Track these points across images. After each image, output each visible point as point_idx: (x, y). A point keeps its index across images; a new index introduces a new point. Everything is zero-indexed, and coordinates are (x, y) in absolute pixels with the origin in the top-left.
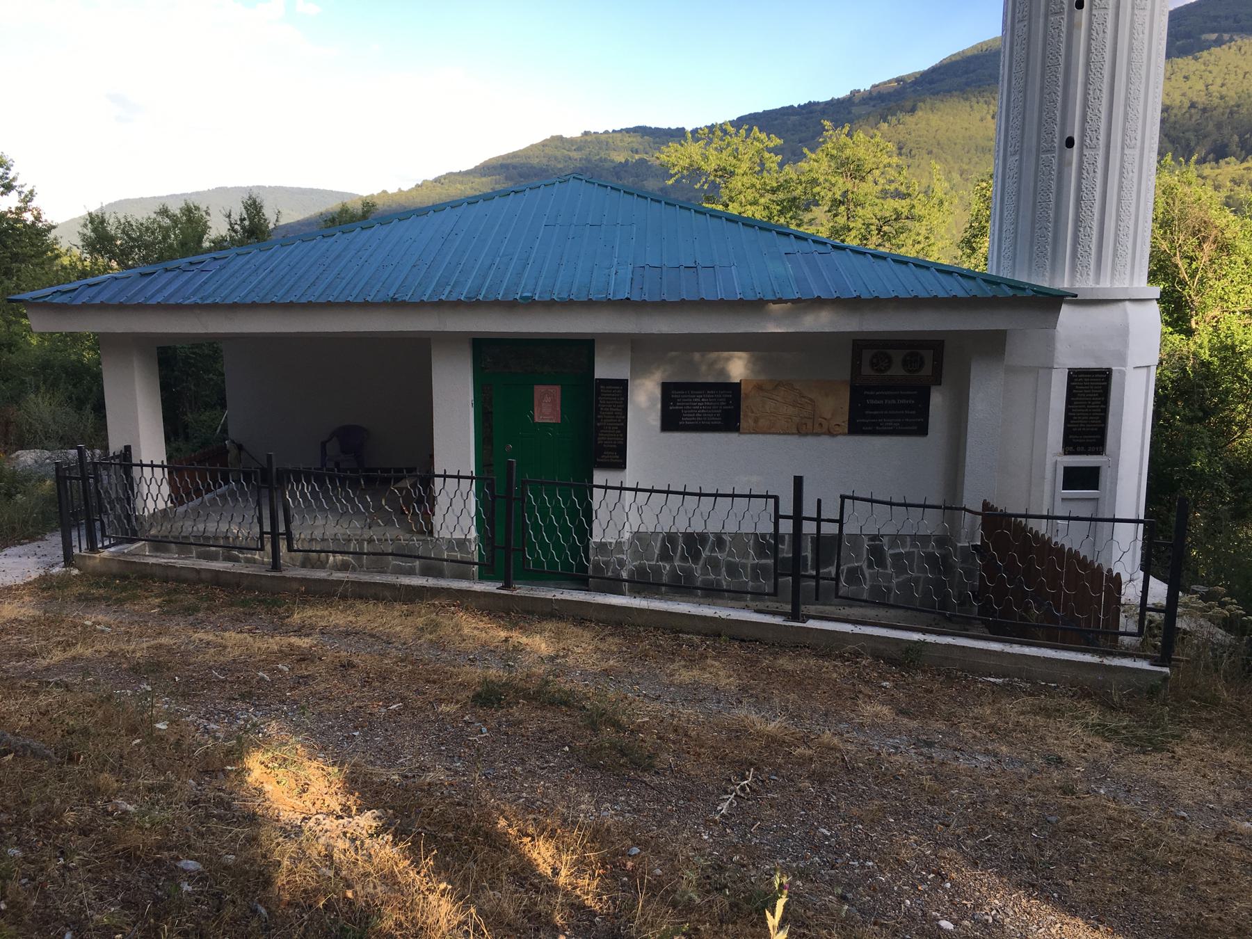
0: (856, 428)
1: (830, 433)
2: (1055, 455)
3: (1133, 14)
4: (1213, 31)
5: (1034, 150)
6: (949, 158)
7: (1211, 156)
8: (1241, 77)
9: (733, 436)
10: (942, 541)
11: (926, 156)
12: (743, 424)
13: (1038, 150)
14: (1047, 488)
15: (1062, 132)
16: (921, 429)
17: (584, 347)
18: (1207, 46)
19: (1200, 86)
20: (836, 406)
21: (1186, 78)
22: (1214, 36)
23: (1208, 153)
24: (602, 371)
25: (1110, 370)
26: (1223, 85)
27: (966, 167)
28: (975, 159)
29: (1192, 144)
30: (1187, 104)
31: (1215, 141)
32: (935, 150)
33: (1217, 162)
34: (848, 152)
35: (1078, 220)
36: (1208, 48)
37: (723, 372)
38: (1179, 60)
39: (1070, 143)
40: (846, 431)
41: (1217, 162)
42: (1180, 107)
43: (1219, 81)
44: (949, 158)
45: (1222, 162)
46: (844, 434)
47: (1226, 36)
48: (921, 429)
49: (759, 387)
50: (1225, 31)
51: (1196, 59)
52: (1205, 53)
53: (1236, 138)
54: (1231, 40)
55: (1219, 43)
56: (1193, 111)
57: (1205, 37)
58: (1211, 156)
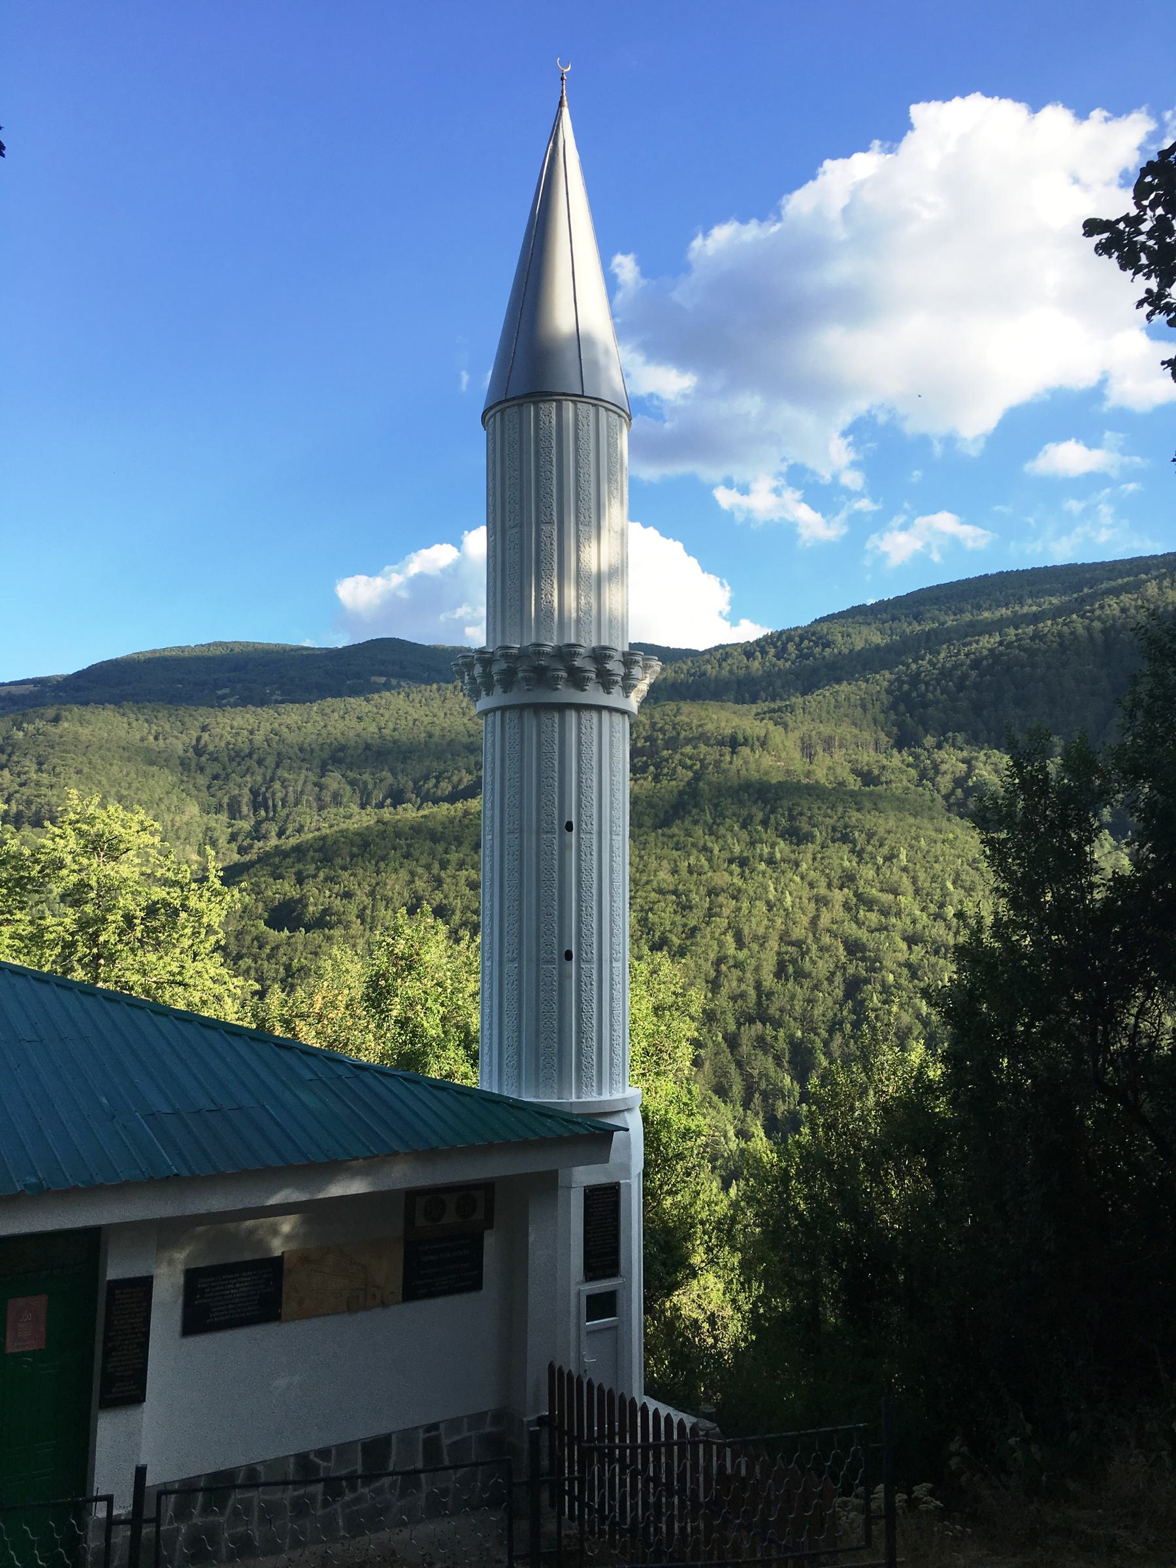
0: (411, 1293)
1: (384, 1304)
2: (578, 1283)
3: (611, 839)
4: (381, 674)
5: (534, 959)
6: (104, 781)
7: (389, 801)
8: (411, 724)
9: (272, 1328)
10: (500, 1416)
11: (74, 776)
12: (285, 1309)
13: (538, 960)
14: (573, 1320)
15: (561, 944)
16: (475, 1284)
17: (92, 1241)
18: (377, 689)
19: (373, 728)
20: (389, 1270)
21: (360, 718)
22: (383, 680)
23: (385, 798)
24: (115, 1270)
25: (618, 1184)
26: (395, 730)
27: (125, 793)
28: (135, 785)
29: (370, 787)
30: (362, 746)
31: (391, 785)
32: (86, 770)
33: (395, 808)
34: (99, 826)
35: (580, 1031)
36: (378, 691)
37: (262, 1244)
38: (352, 700)
39: (568, 956)
40: (400, 1298)
41: (395, 808)
42: (355, 748)
43: (391, 725)
44: (104, 781)
45: (399, 808)
46: (397, 1303)
47: (394, 682)
48: (475, 1284)
49: (304, 1258)
50: (393, 676)
51: (368, 700)
52: (376, 696)
53: (411, 784)
54: (399, 686)
55: (387, 687)
56: (368, 753)
57: (374, 679)
58: (389, 801)
